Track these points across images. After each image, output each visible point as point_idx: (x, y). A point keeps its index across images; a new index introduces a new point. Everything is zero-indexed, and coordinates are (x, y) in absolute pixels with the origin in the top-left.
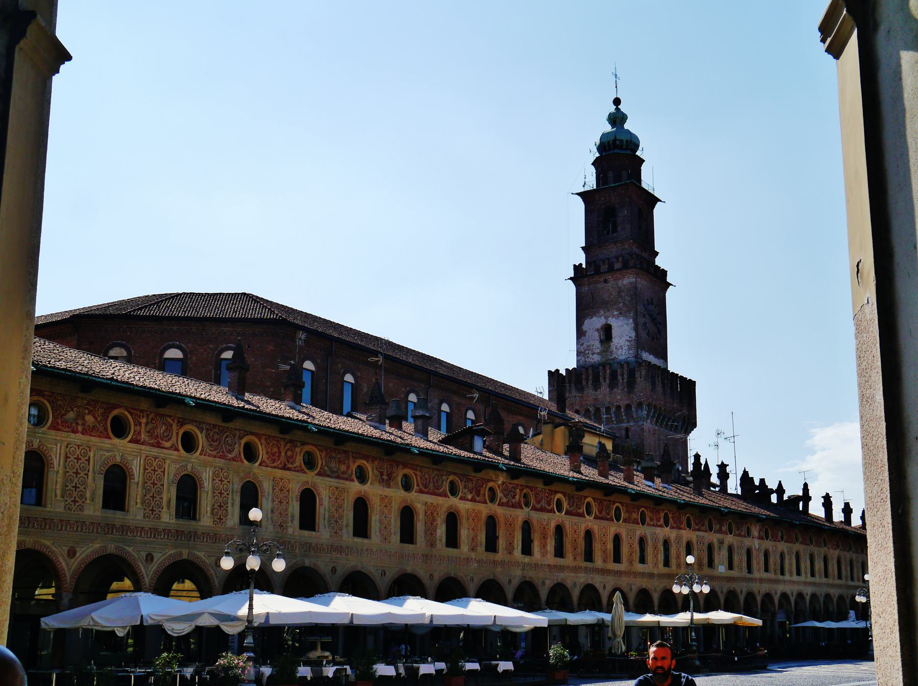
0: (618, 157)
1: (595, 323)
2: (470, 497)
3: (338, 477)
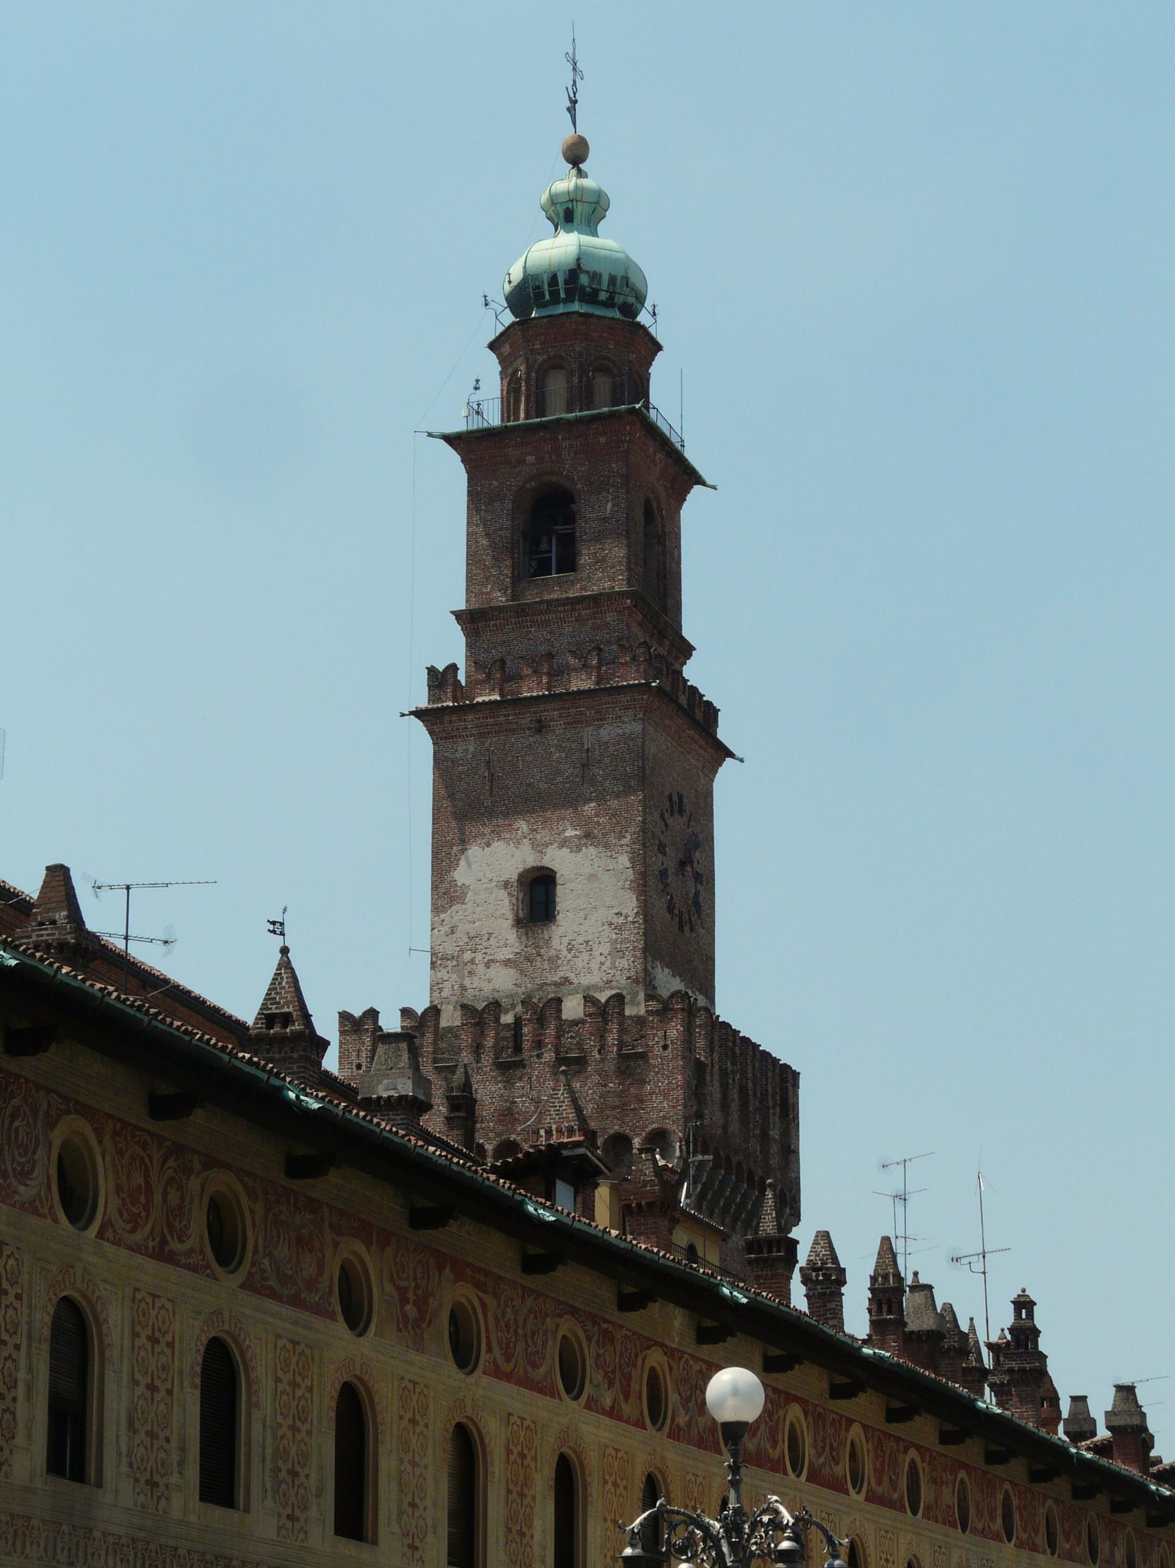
0: (579, 344)
1: (494, 863)
2: (608, 1402)
3: (297, 1302)
